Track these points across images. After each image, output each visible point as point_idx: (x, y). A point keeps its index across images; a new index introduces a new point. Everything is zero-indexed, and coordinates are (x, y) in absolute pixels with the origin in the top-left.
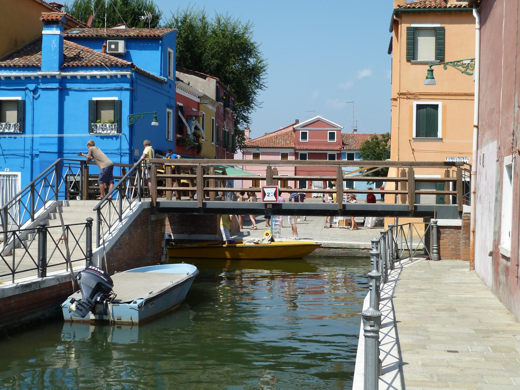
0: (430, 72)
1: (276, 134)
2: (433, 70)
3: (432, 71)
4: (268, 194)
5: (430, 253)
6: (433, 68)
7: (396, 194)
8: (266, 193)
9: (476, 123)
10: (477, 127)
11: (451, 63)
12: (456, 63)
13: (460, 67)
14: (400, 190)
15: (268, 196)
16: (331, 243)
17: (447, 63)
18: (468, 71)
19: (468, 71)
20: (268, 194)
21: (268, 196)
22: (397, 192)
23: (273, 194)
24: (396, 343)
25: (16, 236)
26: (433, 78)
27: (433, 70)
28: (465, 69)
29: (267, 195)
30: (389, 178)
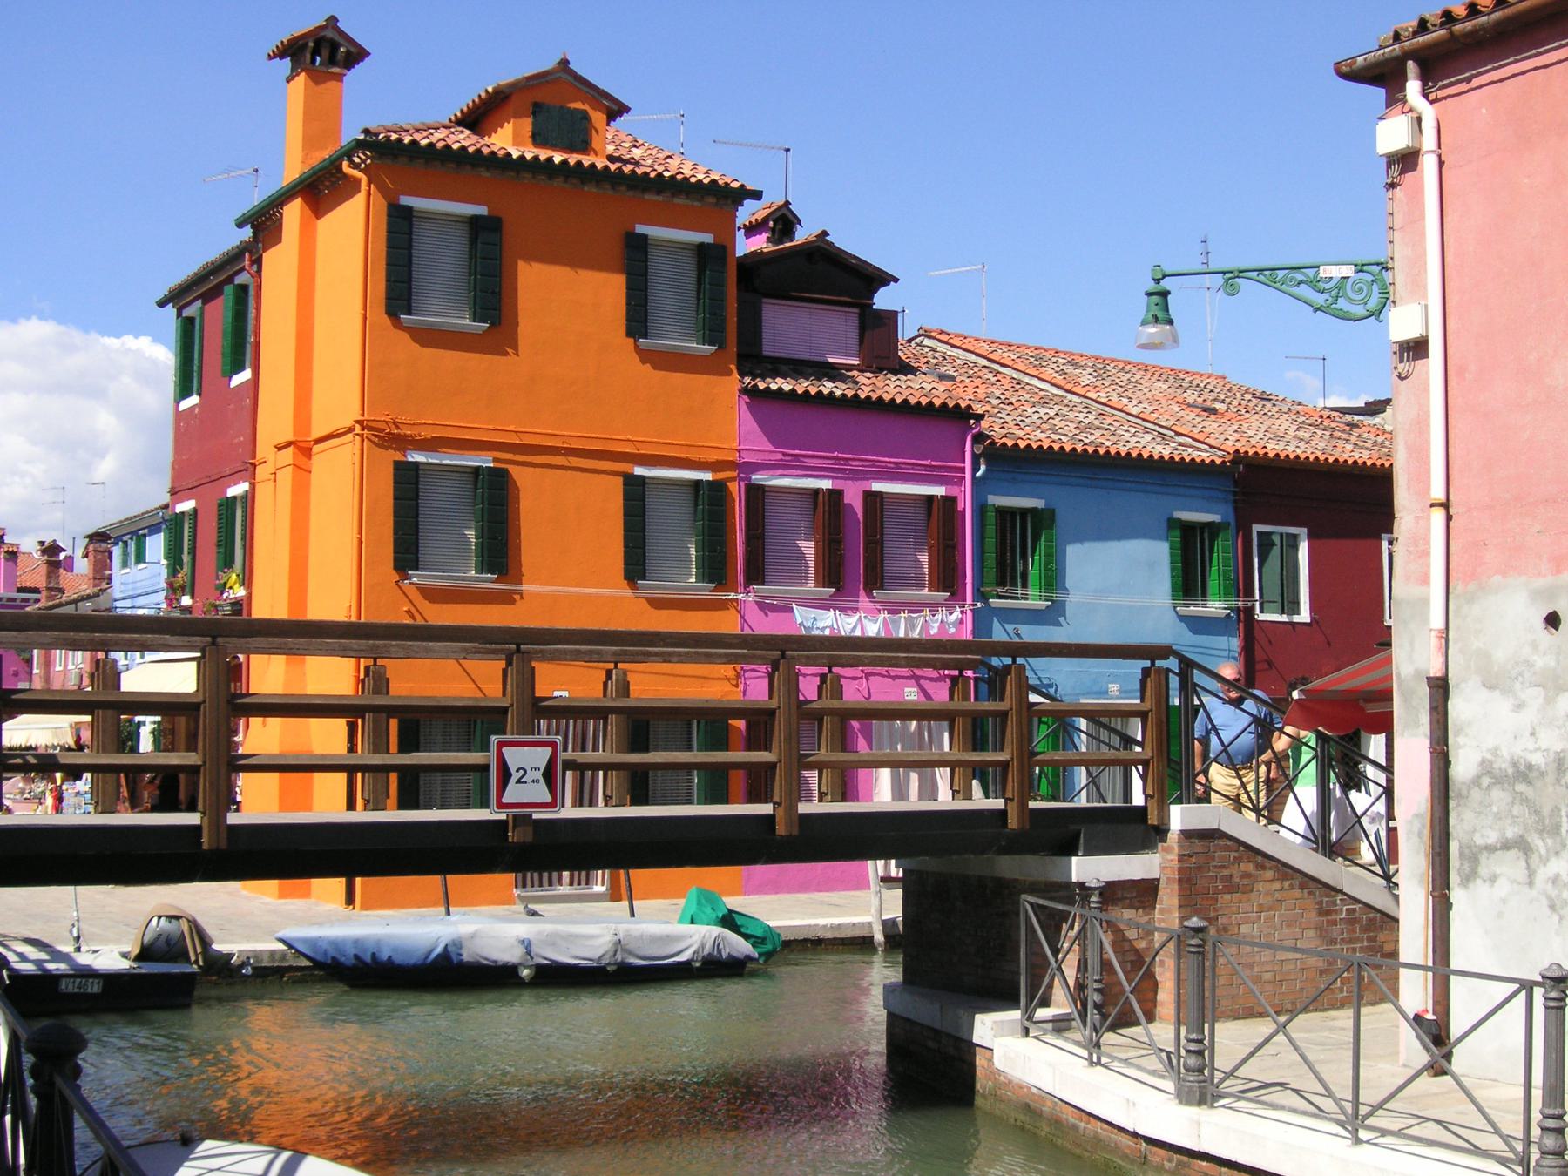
0: (1155, 299)
1: (485, 549)
2: (1169, 293)
3: (1164, 294)
4: (522, 772)
5: (1056, 952)
6: (1166, 284)
7: (350, 770)
8: (513, 769)
9: (1438, 493)
10: (1446, 505)
11: (1260, 271)
12: (1281, 274)
13: (1305, 291)
14: (364, 756)
15: (518, 782)
16: (832, 927)
17: (1241, 272)
18: (1342, 304)
19: (1342, 304)
20: (522, 772)
21: (518, 782)
22: (353, 760)
23: (539, 775)
24: (1381, 1108)
25: (1250, 805)
26: (1170, 322)
27: (1169, 293)
28: (1326, 296)
29: (515, 776)
30: (393, 697)
